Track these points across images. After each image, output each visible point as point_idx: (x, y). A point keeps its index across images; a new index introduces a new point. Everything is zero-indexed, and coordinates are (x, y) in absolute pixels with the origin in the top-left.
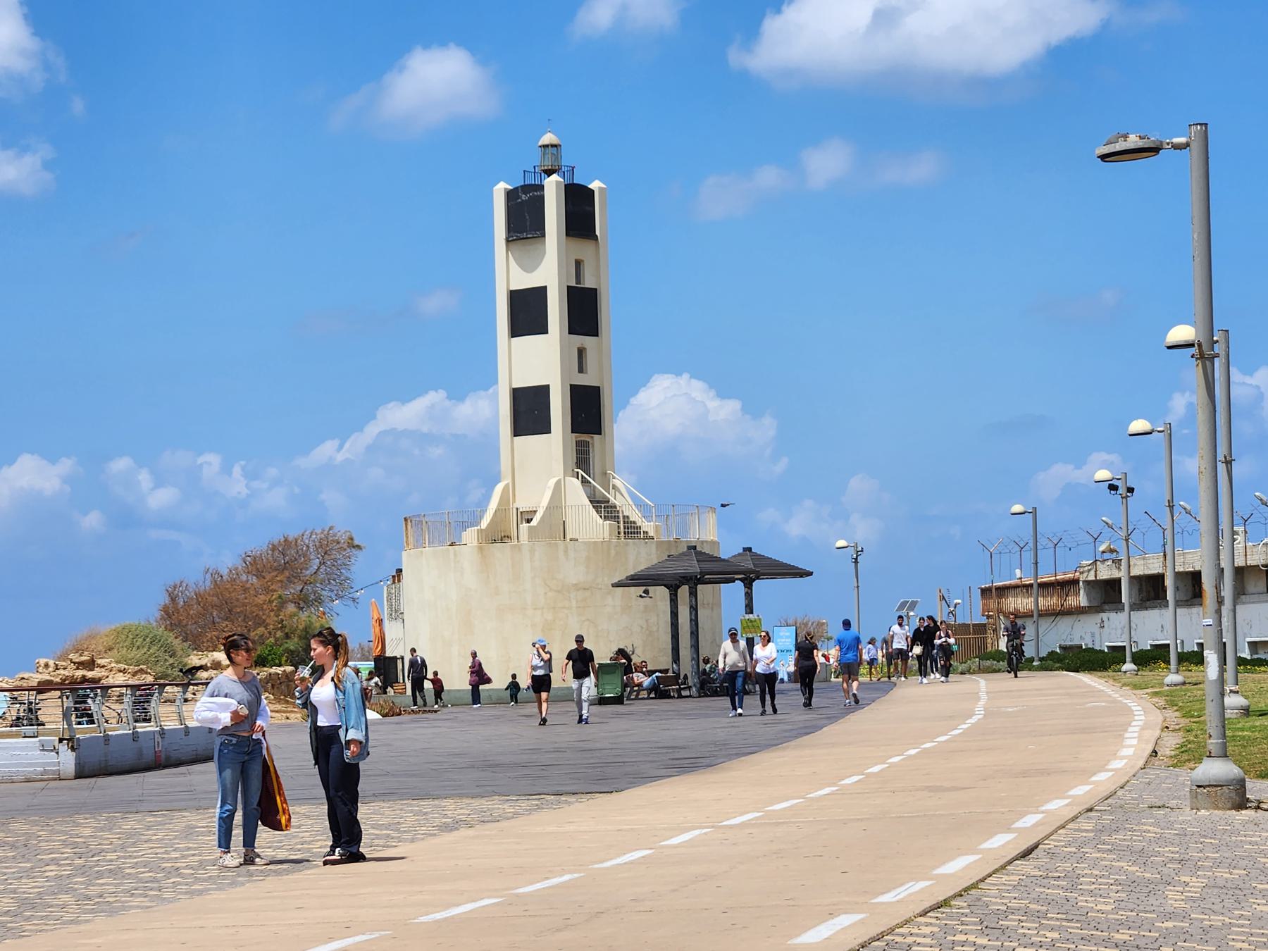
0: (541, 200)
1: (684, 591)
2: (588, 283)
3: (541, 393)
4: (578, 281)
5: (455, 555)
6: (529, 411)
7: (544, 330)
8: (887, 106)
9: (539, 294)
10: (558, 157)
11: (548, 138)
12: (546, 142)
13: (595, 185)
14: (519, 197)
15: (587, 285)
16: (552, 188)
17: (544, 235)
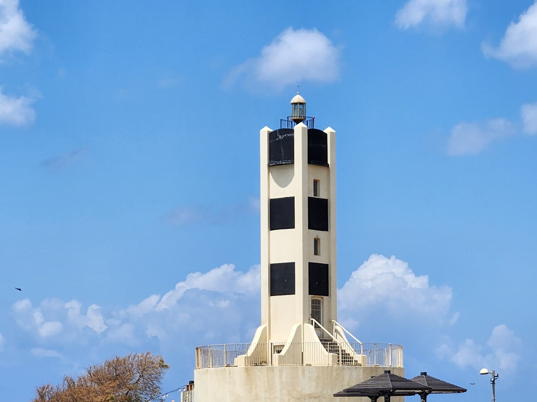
0: (292, 139)
2: (322, 195)
3: (290, 267)
4: (315, 194)
6: (281, 279)
7: (292, 226)
9: (290, 201)
10: (303, 111)
11: (298, 98)
12: (296, 101)
13: (328, 131)
14: (277, 137)
16: (300, 132)
17: (293, 163)
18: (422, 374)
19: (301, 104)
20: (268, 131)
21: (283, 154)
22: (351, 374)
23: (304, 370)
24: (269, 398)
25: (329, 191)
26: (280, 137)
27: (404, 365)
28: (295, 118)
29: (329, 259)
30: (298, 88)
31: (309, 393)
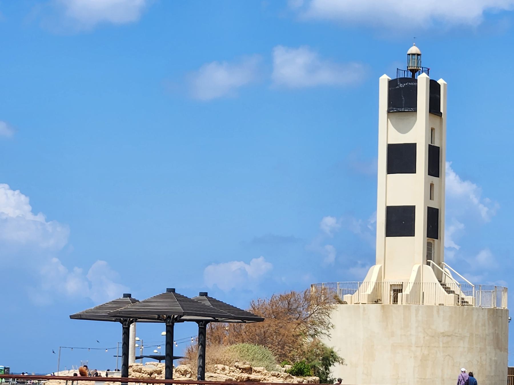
0: (415, 89)
1: (186, 333)
2: (436, 144)
3: (410, 211)
5: (364, 310)
6: (400, 221)
8: (105, 34)
9: (412, 148)
11: (414, 50)
12: (414, 52)
15: (435, 145)
18: (202, 294)
19: (418, 55)
20: (388, 79)
21: (404, 102)
22: (479, 315)
23: (439, 310)
24: (405, 335)
25: (441, 139)
26: (401, 85)
27: (508, 306)
28: (413, 68)
29: (440, 203)
30: (415, 41)
31: (442, 331)
